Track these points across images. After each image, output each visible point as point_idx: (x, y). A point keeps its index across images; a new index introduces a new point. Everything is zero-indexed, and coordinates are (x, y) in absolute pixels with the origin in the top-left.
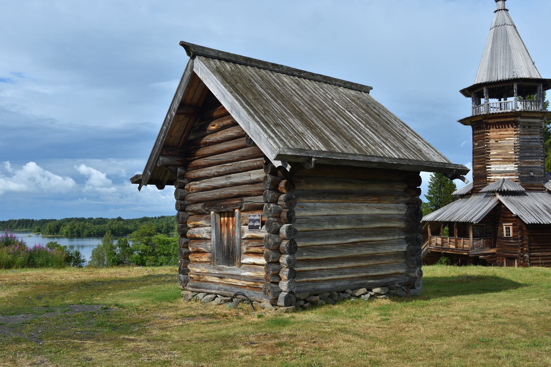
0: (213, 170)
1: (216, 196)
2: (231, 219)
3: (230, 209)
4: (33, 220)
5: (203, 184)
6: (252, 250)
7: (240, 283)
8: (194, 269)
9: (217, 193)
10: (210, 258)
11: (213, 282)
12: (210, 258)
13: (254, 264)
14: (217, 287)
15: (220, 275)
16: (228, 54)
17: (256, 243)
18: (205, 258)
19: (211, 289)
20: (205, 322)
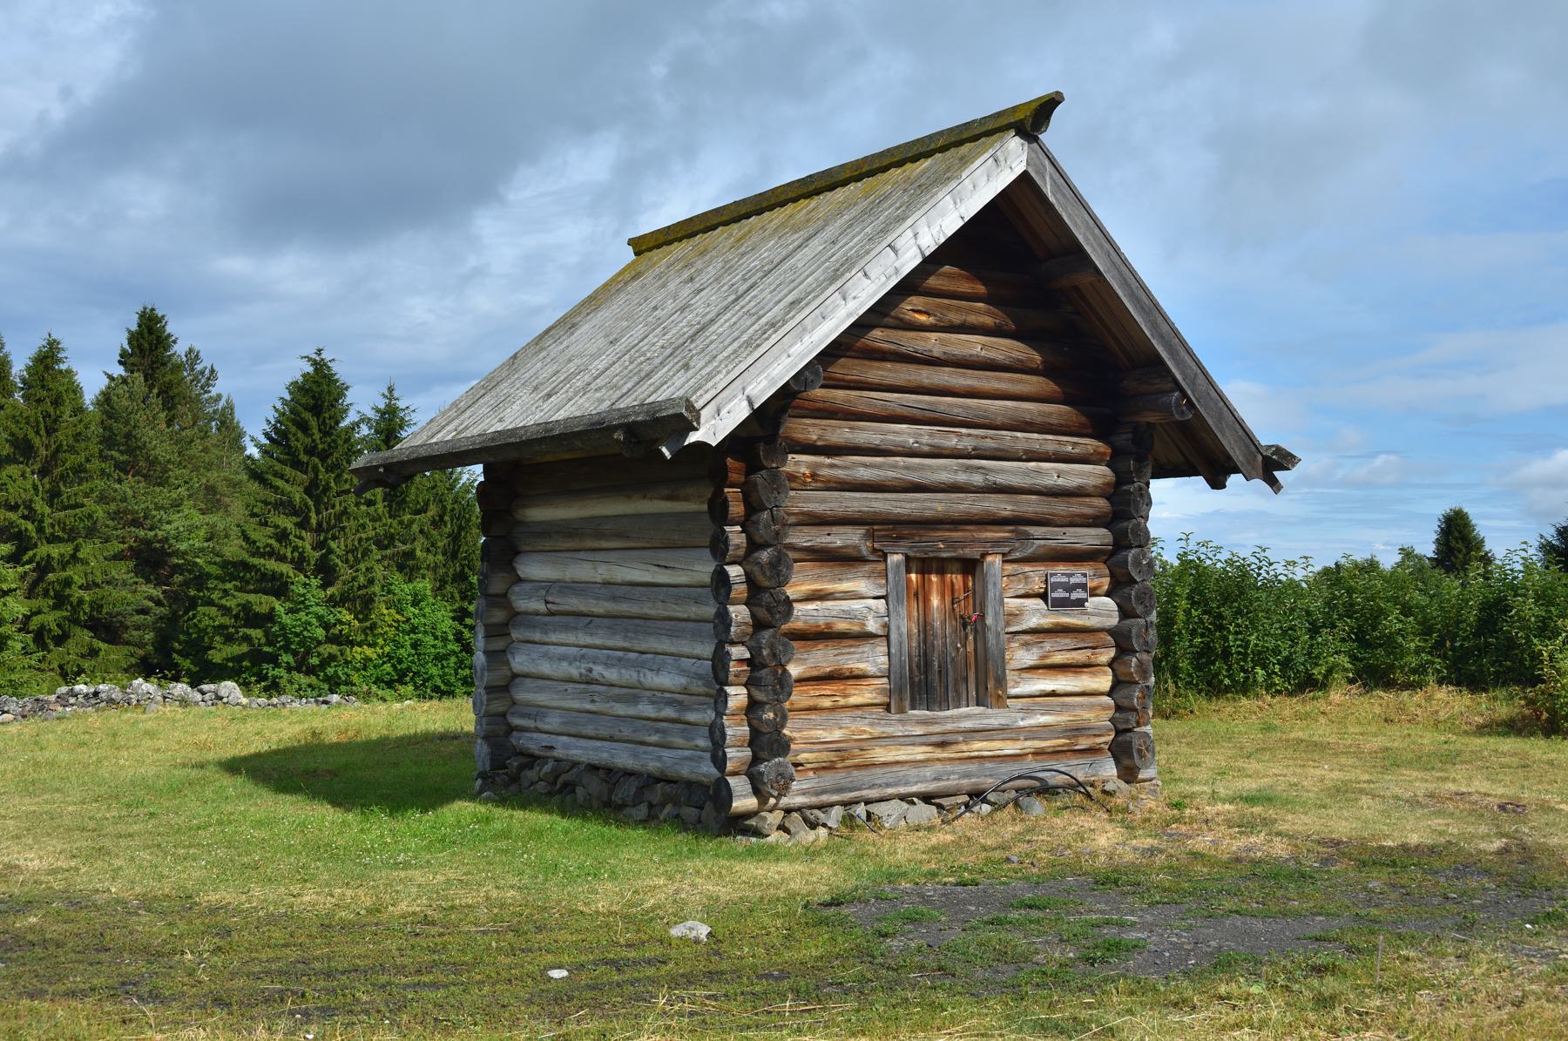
0: (904, 434)
1: (928, 514)
2: (934, 578)
3: (971, 552)
4: (103, 393)
5: (832, 468)
6: (1058, 658)
7: (1010, 748)
8: (810, 734)
9: (937, 505)
10: (881, 691)
11: (897, 763)
12: (881, 691)
13: (1053, 694)
14: (928, 772)
15: (934, 739)
16: (967, 125)
17: (1068, 641)
18: (862, 695)
19: (906, 784)
20: (1421, 788)
